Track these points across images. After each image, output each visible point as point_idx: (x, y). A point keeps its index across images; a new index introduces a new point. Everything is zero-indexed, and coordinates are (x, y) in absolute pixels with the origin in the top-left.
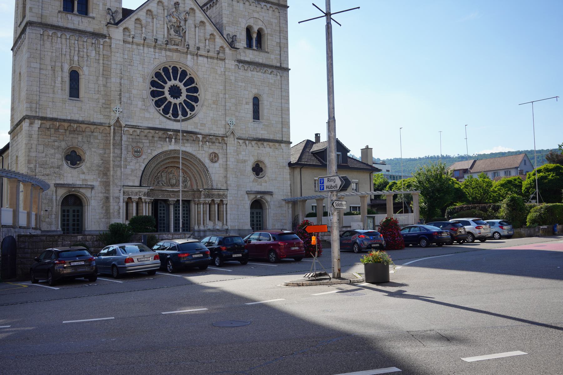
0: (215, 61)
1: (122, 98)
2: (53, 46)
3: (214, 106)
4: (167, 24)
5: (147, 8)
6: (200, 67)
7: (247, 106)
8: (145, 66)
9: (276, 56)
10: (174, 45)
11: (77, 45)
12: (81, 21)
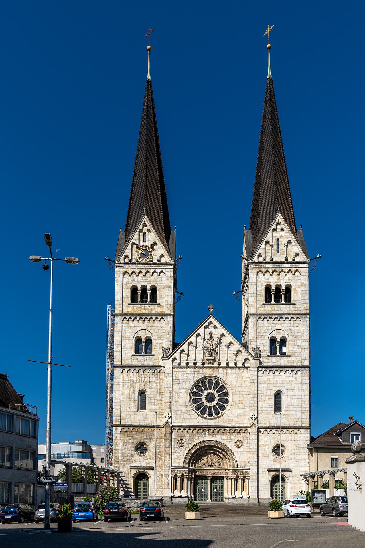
11: (143, 376)
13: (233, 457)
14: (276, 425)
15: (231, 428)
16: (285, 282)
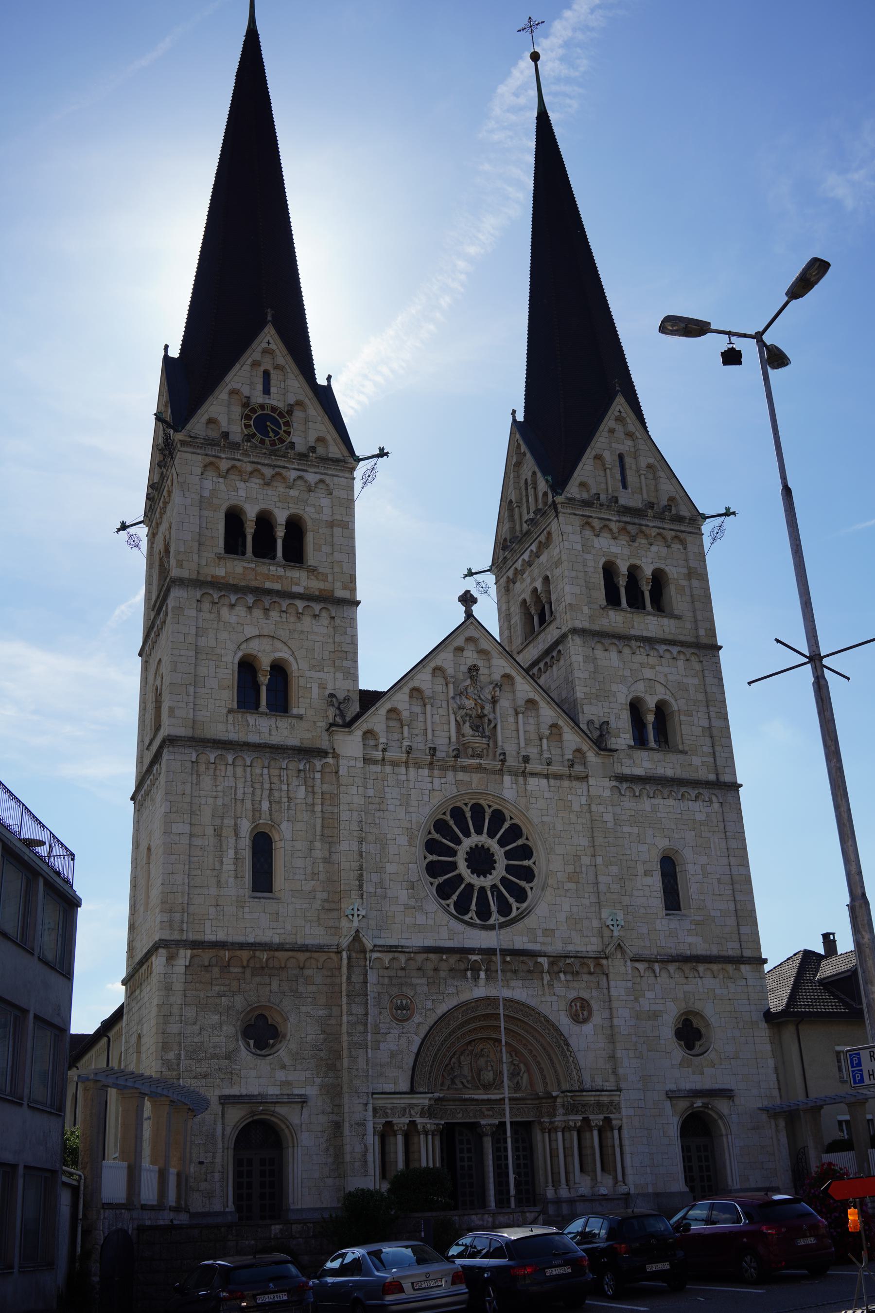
0: (566, 783)
3: (571, 886)
4: (455, 713)
5: (411, 685)
6: (532, 800)
7: (648, 881)
8: (412, 809)
9: (704, 759)
10: (474, 756)
11: (266, 777)
12: (274, 726)
13: (568, 1054)
14: (674, 952)
16: (650, 560)
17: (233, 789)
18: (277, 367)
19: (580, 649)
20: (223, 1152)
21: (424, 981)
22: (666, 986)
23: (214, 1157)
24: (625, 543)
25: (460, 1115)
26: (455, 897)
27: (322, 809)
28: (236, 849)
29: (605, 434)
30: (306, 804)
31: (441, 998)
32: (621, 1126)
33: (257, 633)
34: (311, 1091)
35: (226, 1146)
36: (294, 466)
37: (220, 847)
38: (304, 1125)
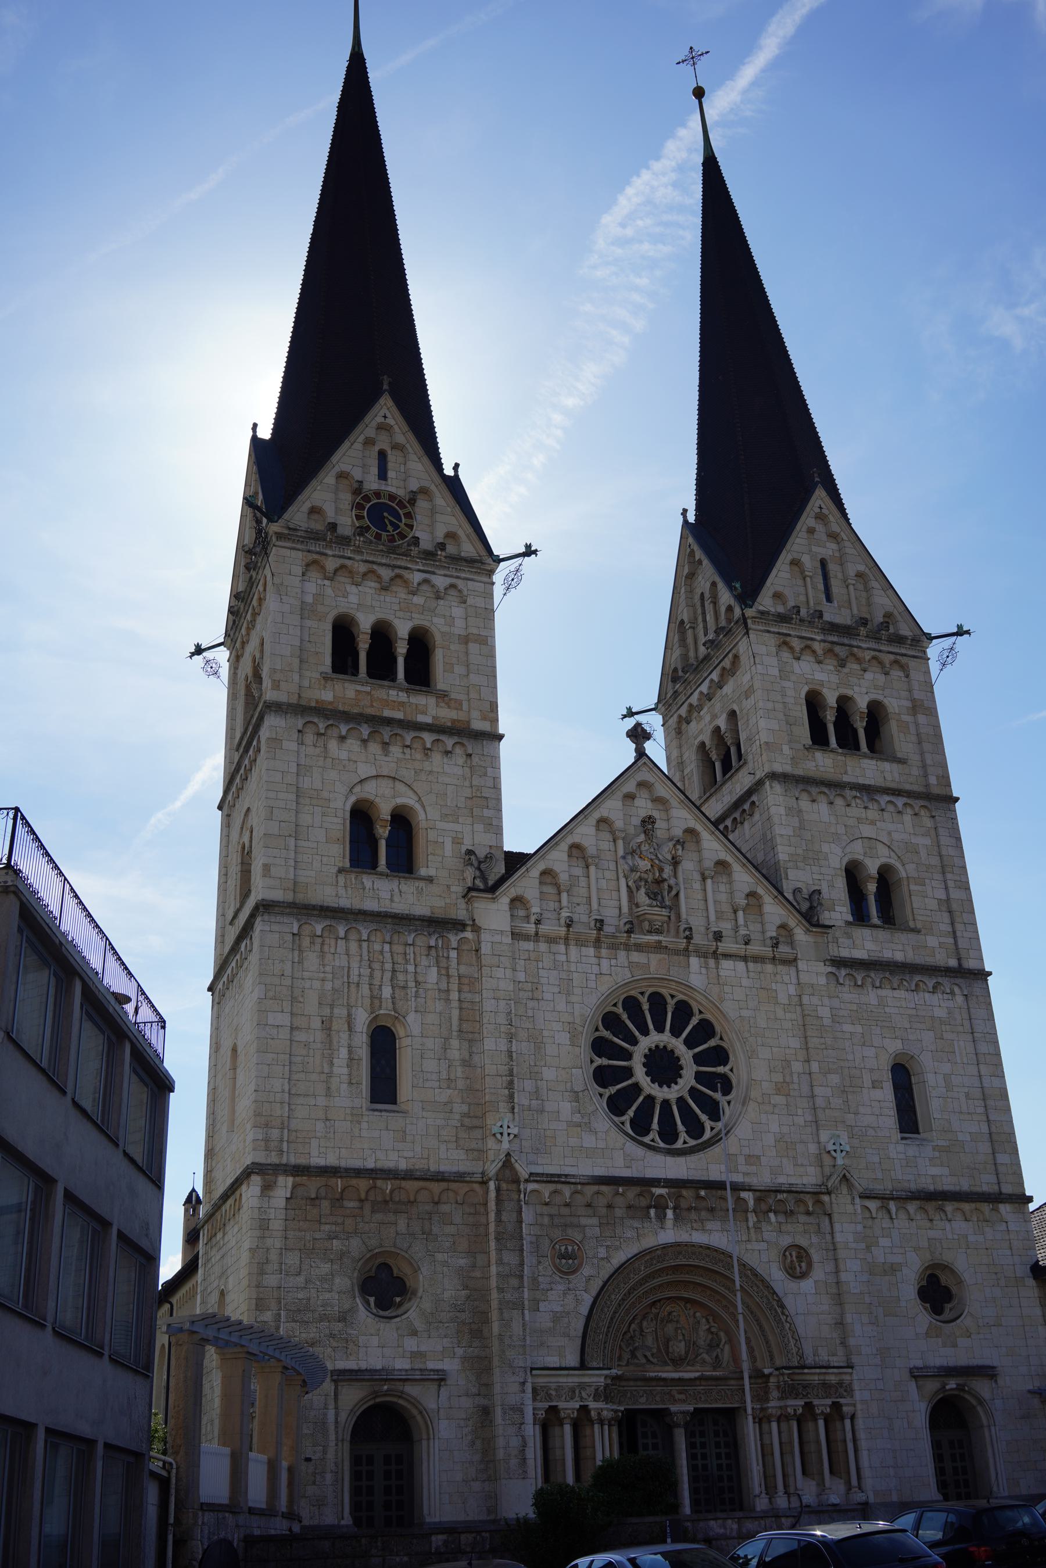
0: (769, 968)
1: (516, 1096)
2: (326, 962)
4: (626, 877)
5: (570, 840)
6: (727, 989)
7: (877, 1094)
9: (942, 940)
10: (651, 932)
11: (388, 955)
12: (396, 890)
13: (783, 1318)
15: (763, 1194)
16: (864, 690)
17: (346, 970)
18: (396, 447)
19: (781, 798)
20: (336, 1445)
21: (595, 1221)
22: (904, 1231)
23: (325, 1452)
24: (832, 668)
25: (643, 1400)
26: (631, 1113)
27: (459, 998)
28: (350, 1047)
29: (803, 534)
30: (439, 990)
31: (618, 1243)
32: (854, 1414)
33: (374, 773)
34: (452, 1365)
35: (340, 1438)
36: (418, 567)
37: (329, 1043)
38: (441, 1411)
